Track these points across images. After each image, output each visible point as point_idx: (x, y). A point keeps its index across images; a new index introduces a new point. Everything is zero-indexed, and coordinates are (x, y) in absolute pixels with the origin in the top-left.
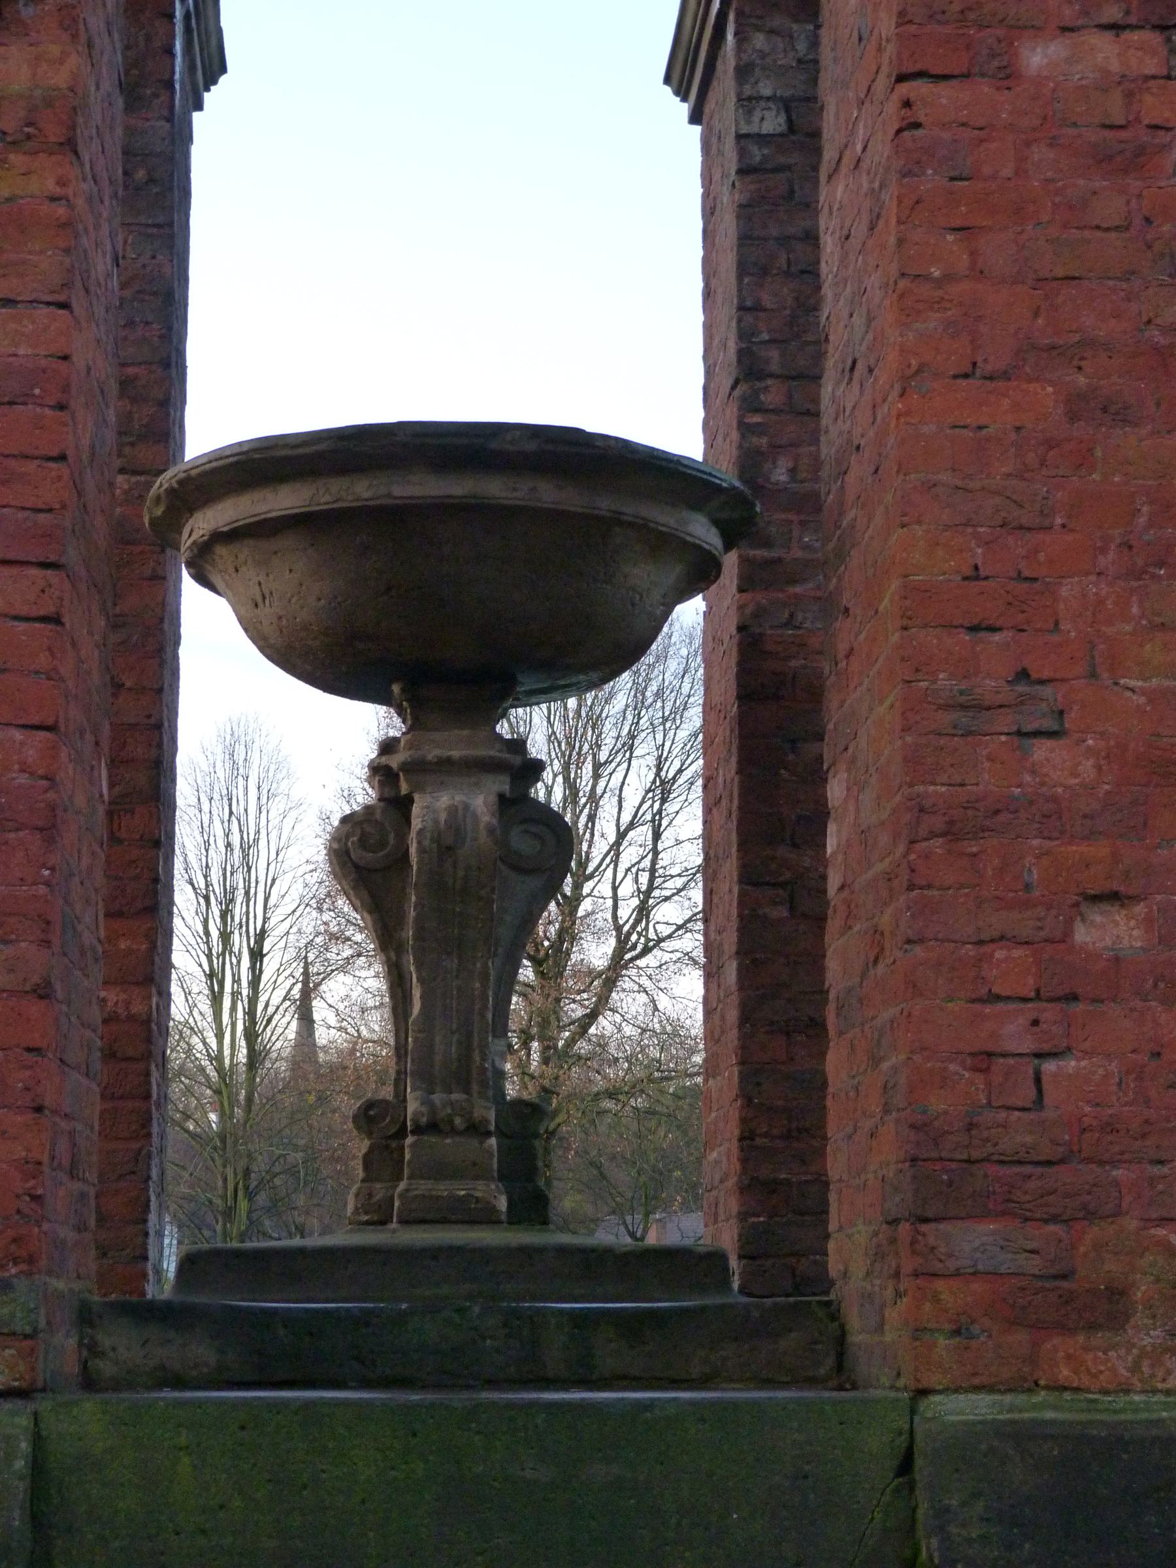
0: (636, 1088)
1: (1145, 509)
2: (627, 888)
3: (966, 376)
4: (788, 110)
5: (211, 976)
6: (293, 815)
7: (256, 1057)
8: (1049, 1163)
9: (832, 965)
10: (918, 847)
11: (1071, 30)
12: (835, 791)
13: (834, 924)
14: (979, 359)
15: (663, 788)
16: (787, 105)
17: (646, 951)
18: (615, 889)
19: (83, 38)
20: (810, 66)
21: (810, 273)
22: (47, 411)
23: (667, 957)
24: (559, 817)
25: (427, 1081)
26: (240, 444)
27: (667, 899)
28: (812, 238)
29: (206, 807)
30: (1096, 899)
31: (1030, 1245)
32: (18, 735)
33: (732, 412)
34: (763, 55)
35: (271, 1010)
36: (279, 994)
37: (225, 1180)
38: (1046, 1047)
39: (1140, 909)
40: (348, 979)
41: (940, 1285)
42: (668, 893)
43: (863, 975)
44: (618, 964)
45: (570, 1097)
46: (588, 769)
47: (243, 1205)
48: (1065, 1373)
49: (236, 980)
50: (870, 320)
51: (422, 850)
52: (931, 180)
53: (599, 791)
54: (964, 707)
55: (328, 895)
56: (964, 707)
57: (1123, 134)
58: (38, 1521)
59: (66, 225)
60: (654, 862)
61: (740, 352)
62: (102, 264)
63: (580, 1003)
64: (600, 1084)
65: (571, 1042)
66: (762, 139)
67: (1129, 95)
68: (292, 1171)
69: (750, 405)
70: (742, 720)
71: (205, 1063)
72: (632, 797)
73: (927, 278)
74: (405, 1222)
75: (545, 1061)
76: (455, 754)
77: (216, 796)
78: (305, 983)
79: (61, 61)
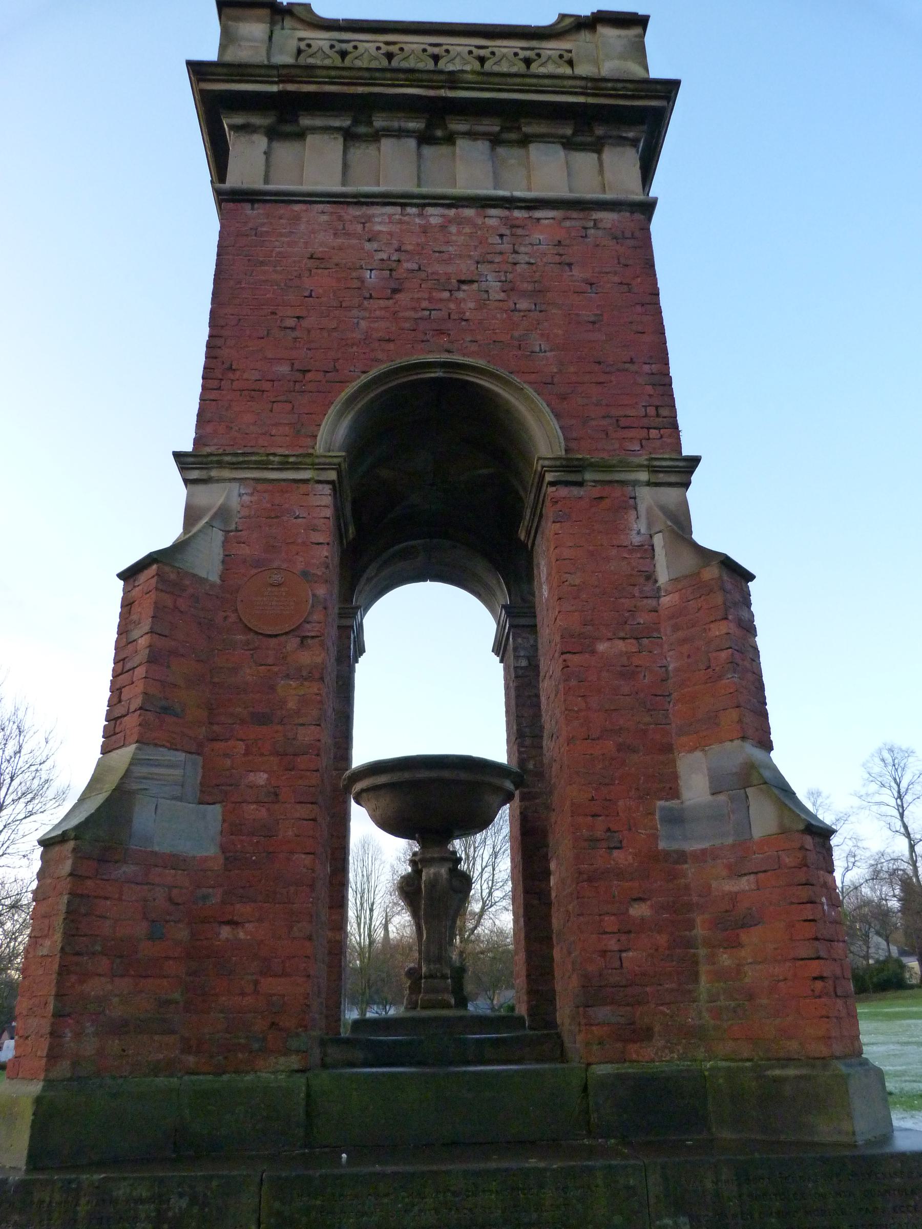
0: (489, 950)
1: (642, 778)
2: (485, 886)
3: (586, 739)
4: (529, 660)
5: (357, 917)
6: (382, 865)
7: (371, 943)
8: (625, 986)
9: (554, 921)
10: (580, 885)
11: (611, 639)
12: (553, 866)
13: (554, 909)
14: (590, 734)
15: (495, 855)
16: (528, 658)
17: (491, 906)
18: (481, 887)
19: (326, 648)
20: (535, 647)
21: (538, 705)
22: (313, 757)
23: (498, 908)
24: (466, 873)
25: (429, 961)
26: (370, 762)
27: (497, 889)
28: (537, 696)
29: (356, 863)
30: (635, 900)
31: (621, 1014)
32: (303, 856)
33: (515, 747)
34: (520, 644)
35: (376, 928)
36: (378, 922)
37: (362, 983)
38: (623, 949)
39: (649, 903)
40: (400, 917)
41: (594, 1028)
42: (497, 887)
43: (564, 926)
44: (483, 911)
45: (469, 954)
46: (472, 849)
47: (367, 991)
48: (634, 1056)
49: (365, 918)
50: (557, 722)
51: (425, 886)
52: (573, 682)
53: (476, 856)
54: (591, 840)
55: (393, 890)
56: (591, 840)
57: (628, 668)
58: (308, 1114)
59: (321, 702)
60: (493, 878)
61: (517, 730)
62: (330, 711)
63: (472, 923)
64: (478, 949)
65: (469, 935)
66: (522, 668)
67: (628, 658)
68: (383, 980)
69: (521, 745)
70: (522, 840)
71: (356, 945)
72: (486, 857)
73: (574, 710)
74: (423, 1008)
75: (461, 942)
76: (436, 855)
77: (359, 860)
78: (386, 919)
79: (320, 655)
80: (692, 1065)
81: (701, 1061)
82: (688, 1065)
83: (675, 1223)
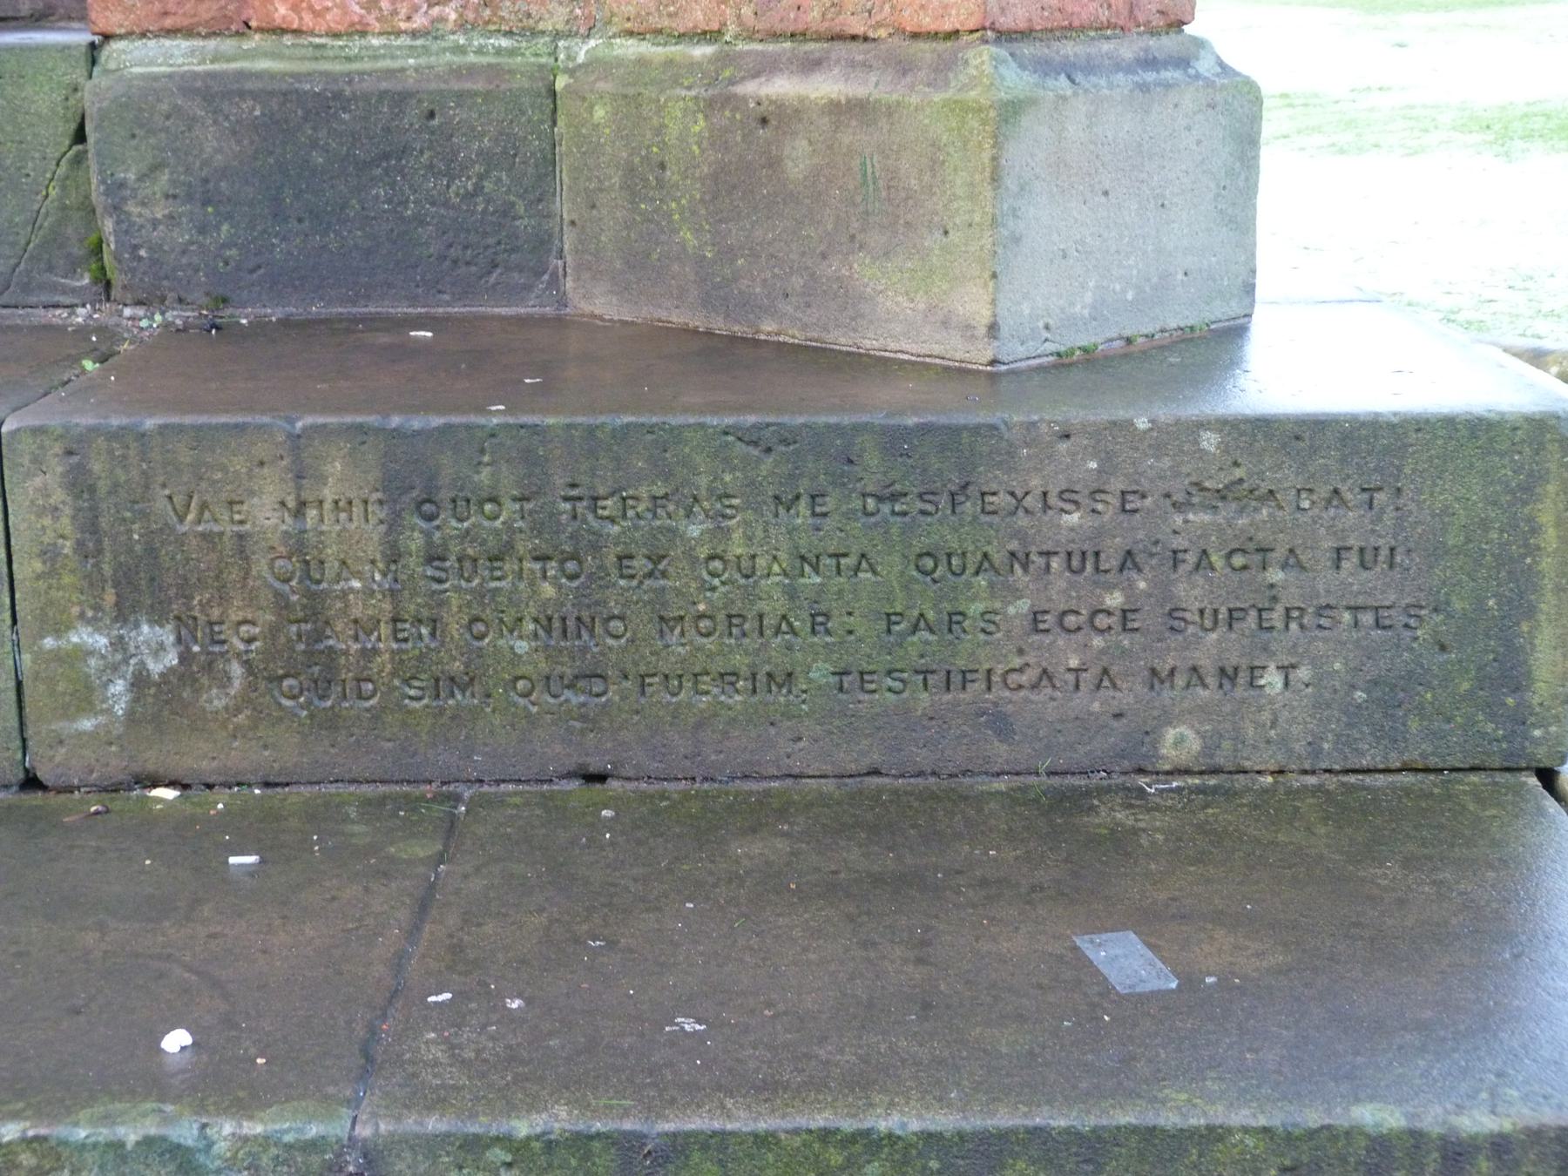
80: (512, 52)
81: (557, 35)
82: (499, 51)
83: (119, 644)
